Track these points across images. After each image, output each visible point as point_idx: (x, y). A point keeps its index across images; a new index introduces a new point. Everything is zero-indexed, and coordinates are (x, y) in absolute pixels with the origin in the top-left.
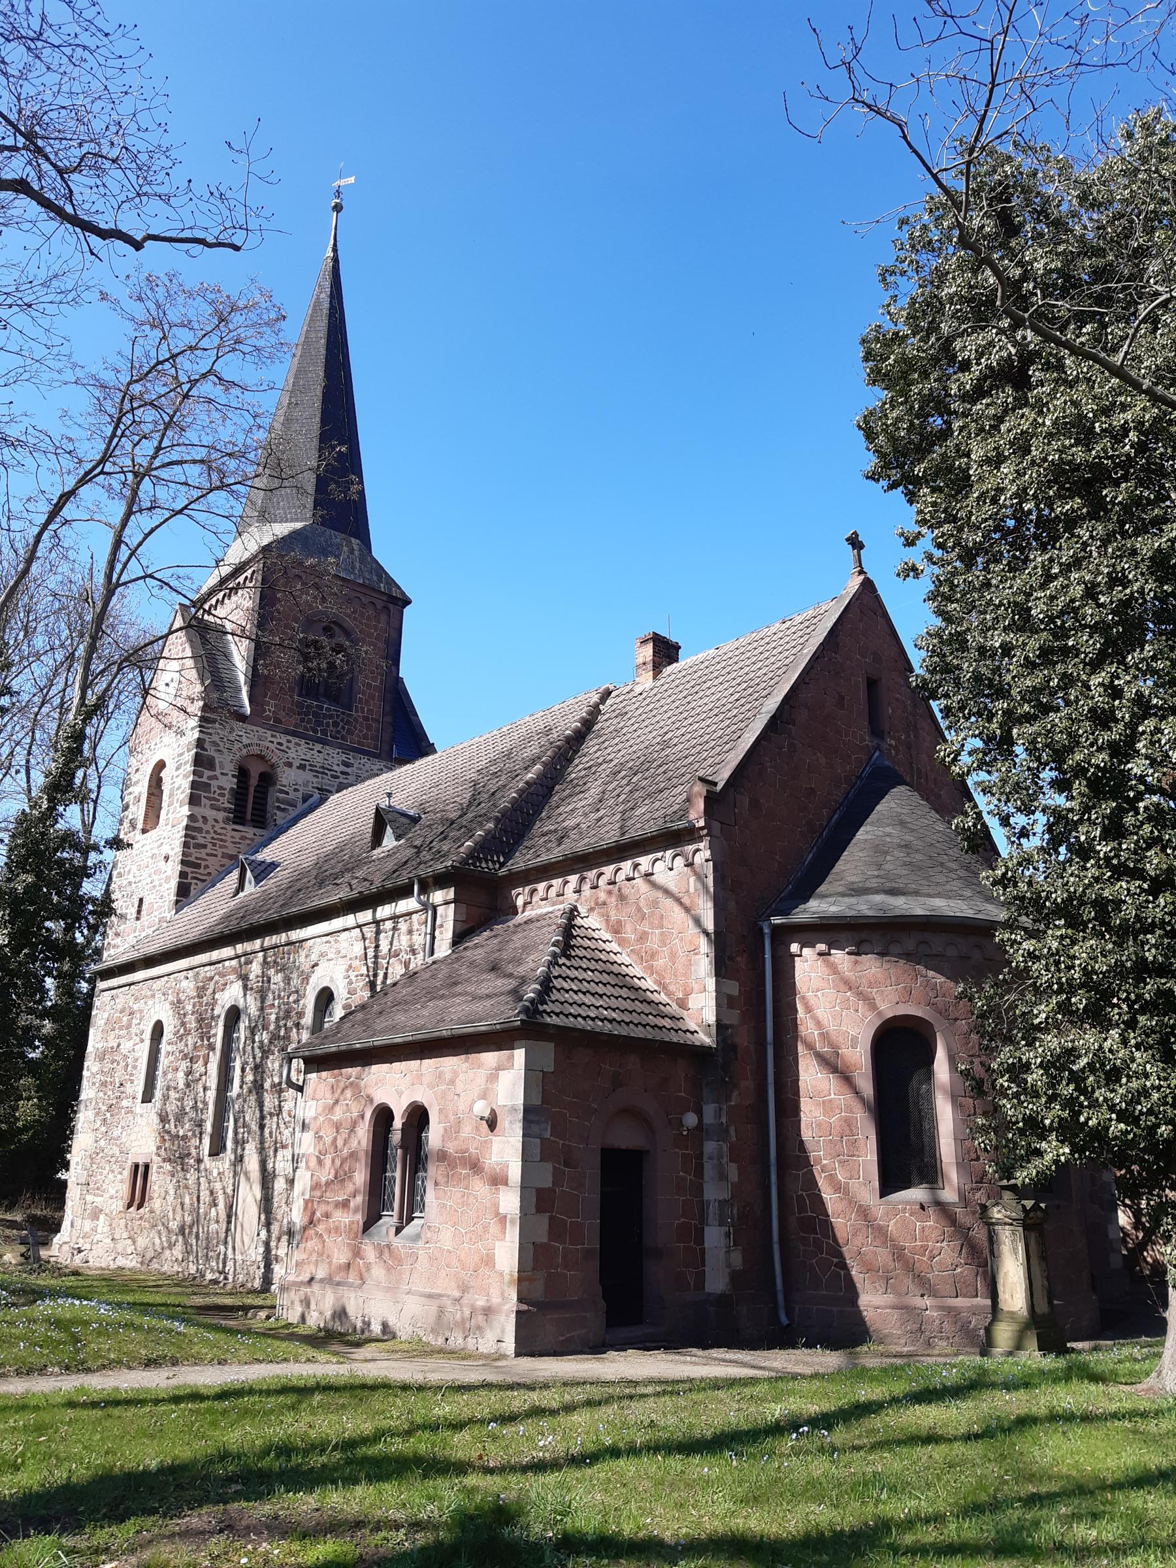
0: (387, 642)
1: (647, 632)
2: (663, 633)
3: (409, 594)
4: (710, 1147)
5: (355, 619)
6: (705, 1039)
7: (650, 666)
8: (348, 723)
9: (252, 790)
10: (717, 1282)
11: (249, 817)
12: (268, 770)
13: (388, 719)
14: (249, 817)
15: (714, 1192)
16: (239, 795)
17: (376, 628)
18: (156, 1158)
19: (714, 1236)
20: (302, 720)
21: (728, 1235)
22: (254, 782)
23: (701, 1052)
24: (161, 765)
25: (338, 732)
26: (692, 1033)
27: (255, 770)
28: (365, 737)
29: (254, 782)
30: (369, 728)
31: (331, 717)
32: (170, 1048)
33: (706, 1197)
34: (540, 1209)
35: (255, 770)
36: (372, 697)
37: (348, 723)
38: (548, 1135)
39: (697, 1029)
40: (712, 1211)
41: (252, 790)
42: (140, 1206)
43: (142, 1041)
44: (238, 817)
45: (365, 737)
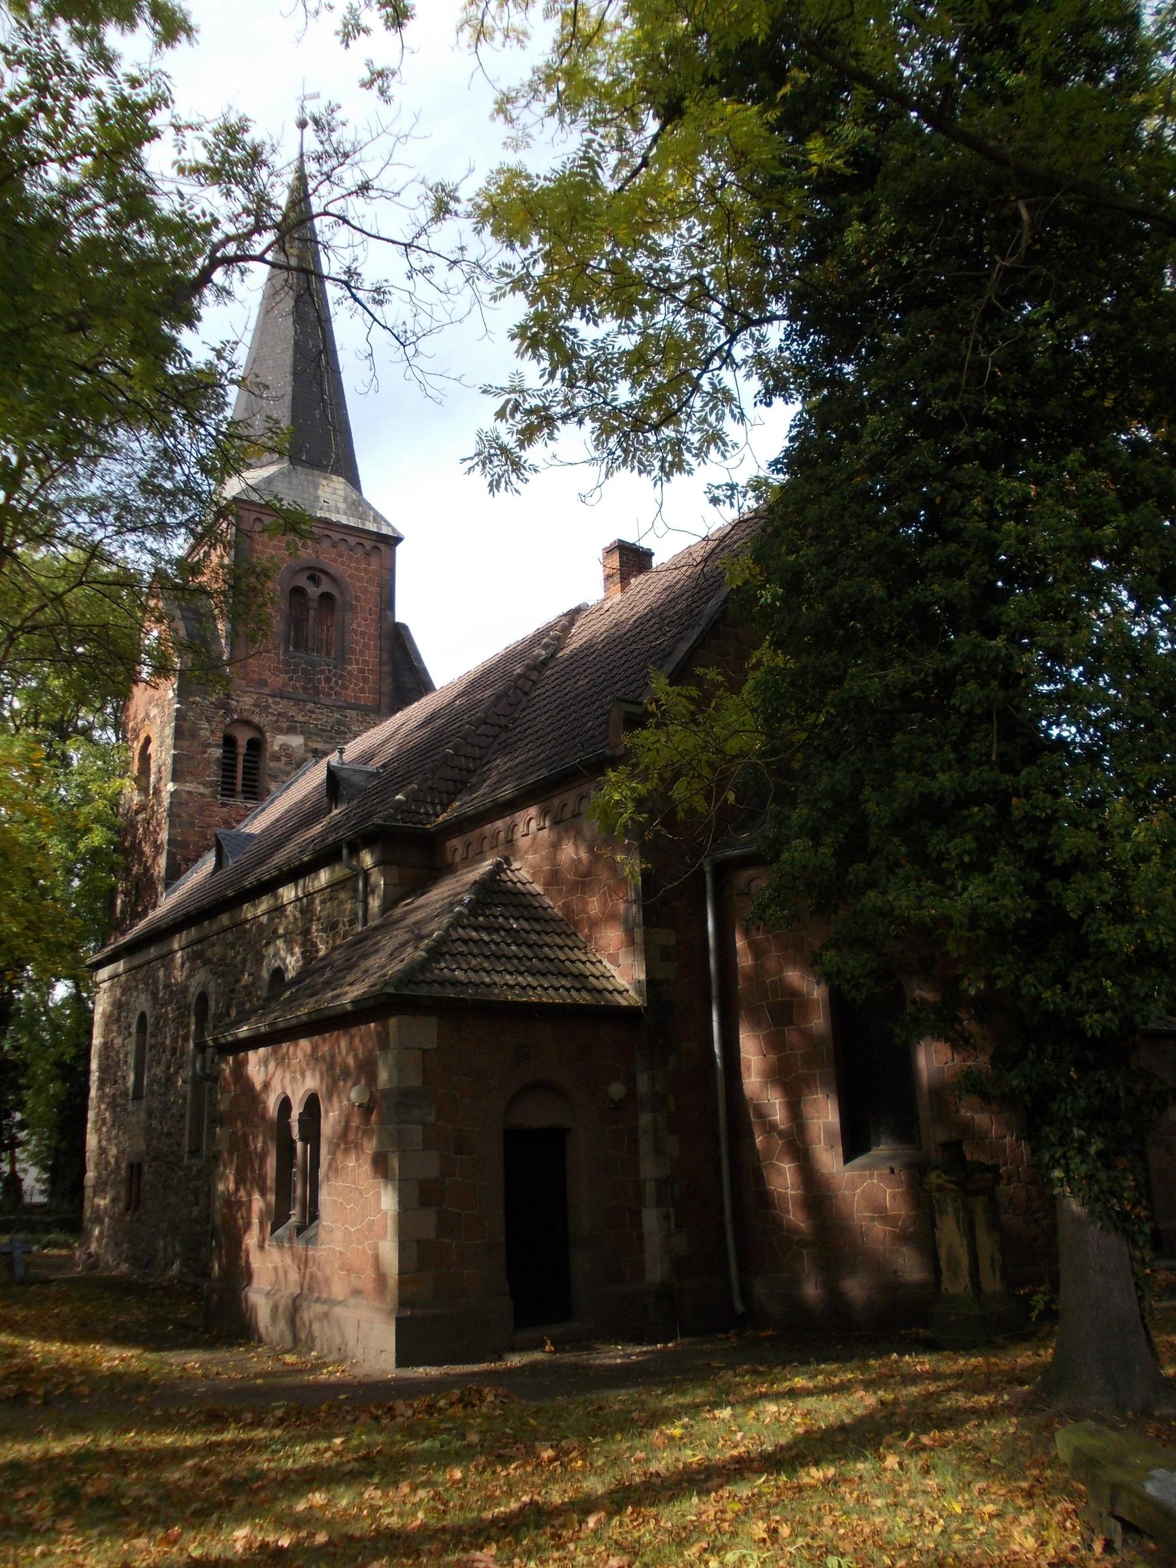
0: (380, 586)
1: (608, 541)
2: (630, 538)
3: (401, 529)
4: (645, 1119)
5: (343, 563)
6: (633, 998)
7: (617, 578)
8: (341, 677)
9: (241, 759)
10: (656, 1270)
11: (239, 788)
12: (256, 735)
13: (386, 669)
14: (239, 788)
15: (649, 1170)
16: (227, 766)
17: (366, 571)
18: (147, 1158)
19: (651, 1219)
20: (291, 679)
21: (667, 1217)
22: (242, 750)
23: (629, 1015)
24: (148, 740)
25: (331, 688)
26: (620, 993)
27: (243, 737)
28: (362, 691)
29: (242, 750)
30: (366, 680)
31: (322, 672)
32: (153, 1041)
33: (642, 1176)
34: (424, 1203)
35: (243, 737)
36: (367, 646)
37: (341, 677)
38: (432, 1119)
39: (628, 986)
40: (650, 1190)
41: (241, 759)
42: (136, 1209)
43: (130, 1034)
44: (228, 789)
45: (362, 691)
